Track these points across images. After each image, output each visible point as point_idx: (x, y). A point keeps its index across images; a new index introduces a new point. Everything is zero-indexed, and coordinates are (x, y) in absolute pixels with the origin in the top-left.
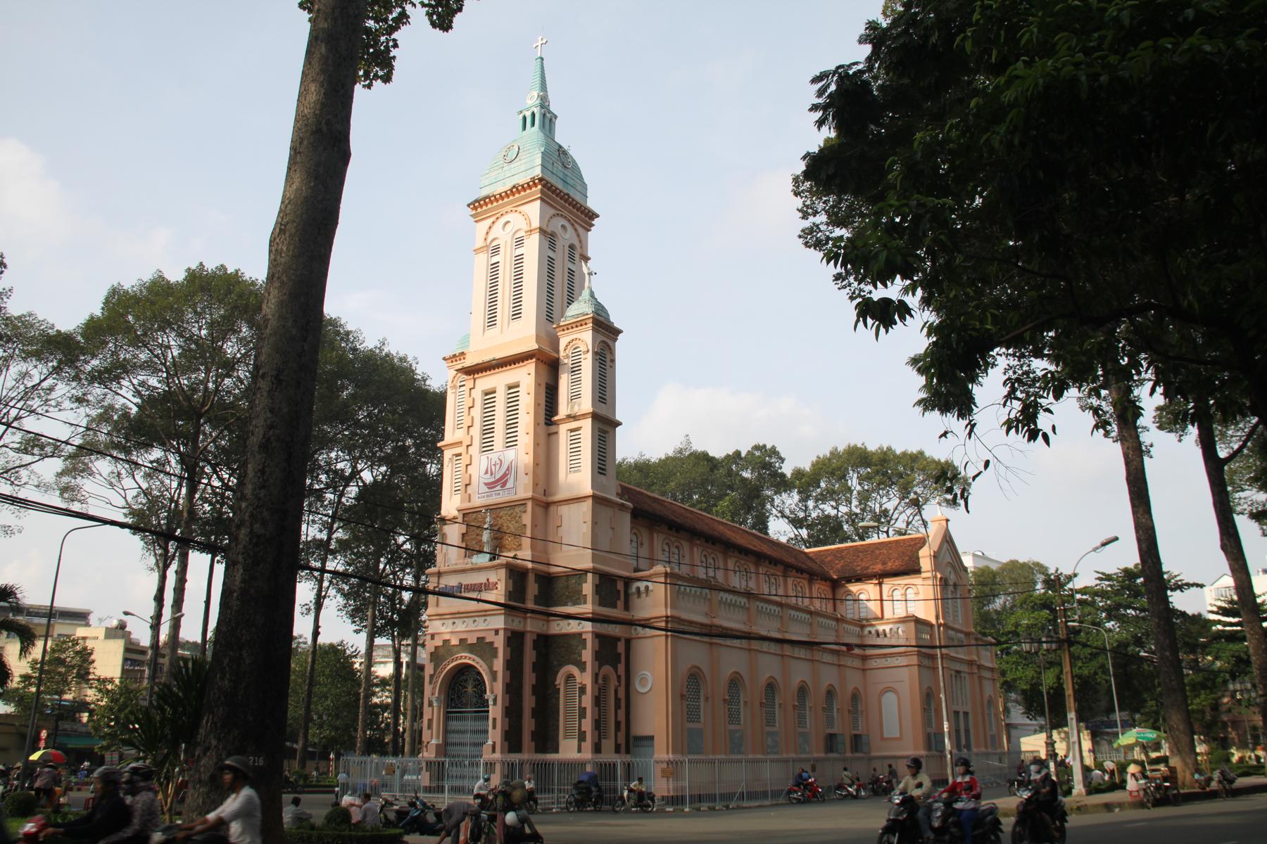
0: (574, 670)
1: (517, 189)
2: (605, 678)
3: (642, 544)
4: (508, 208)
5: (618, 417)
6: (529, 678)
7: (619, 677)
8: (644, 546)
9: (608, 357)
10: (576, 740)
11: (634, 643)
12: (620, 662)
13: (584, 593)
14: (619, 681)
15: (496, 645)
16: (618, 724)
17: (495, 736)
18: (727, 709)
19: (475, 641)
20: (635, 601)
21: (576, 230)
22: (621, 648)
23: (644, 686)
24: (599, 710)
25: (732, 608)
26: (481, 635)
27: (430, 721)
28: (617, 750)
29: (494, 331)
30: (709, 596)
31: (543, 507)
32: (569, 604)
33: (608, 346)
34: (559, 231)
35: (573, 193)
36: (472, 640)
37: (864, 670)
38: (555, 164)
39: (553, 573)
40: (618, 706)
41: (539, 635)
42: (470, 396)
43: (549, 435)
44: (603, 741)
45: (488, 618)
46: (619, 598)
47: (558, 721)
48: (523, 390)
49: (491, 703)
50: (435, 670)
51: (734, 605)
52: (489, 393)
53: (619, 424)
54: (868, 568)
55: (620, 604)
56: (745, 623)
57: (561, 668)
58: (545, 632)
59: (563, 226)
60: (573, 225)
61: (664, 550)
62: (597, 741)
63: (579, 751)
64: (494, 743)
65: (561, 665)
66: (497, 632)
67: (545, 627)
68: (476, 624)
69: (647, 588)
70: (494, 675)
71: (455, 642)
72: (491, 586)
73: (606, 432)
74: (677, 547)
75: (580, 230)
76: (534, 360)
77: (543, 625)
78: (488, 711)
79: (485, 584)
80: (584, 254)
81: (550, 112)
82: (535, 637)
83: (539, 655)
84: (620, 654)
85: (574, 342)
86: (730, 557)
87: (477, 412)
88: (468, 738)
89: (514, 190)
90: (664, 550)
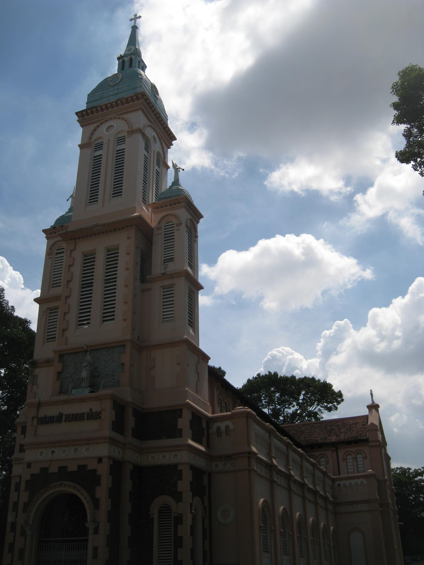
1: (122, 102)
13: (179, 427)
19: (75, 469)
43: (143, 291)
49: (91, 531)
54: (326, 438)
59: (154, 137)
66: (100, 460)
69: (227, 427)
71: (54, 469)
78: (87, 540)
87: (77, 270)
89: (119, 102)
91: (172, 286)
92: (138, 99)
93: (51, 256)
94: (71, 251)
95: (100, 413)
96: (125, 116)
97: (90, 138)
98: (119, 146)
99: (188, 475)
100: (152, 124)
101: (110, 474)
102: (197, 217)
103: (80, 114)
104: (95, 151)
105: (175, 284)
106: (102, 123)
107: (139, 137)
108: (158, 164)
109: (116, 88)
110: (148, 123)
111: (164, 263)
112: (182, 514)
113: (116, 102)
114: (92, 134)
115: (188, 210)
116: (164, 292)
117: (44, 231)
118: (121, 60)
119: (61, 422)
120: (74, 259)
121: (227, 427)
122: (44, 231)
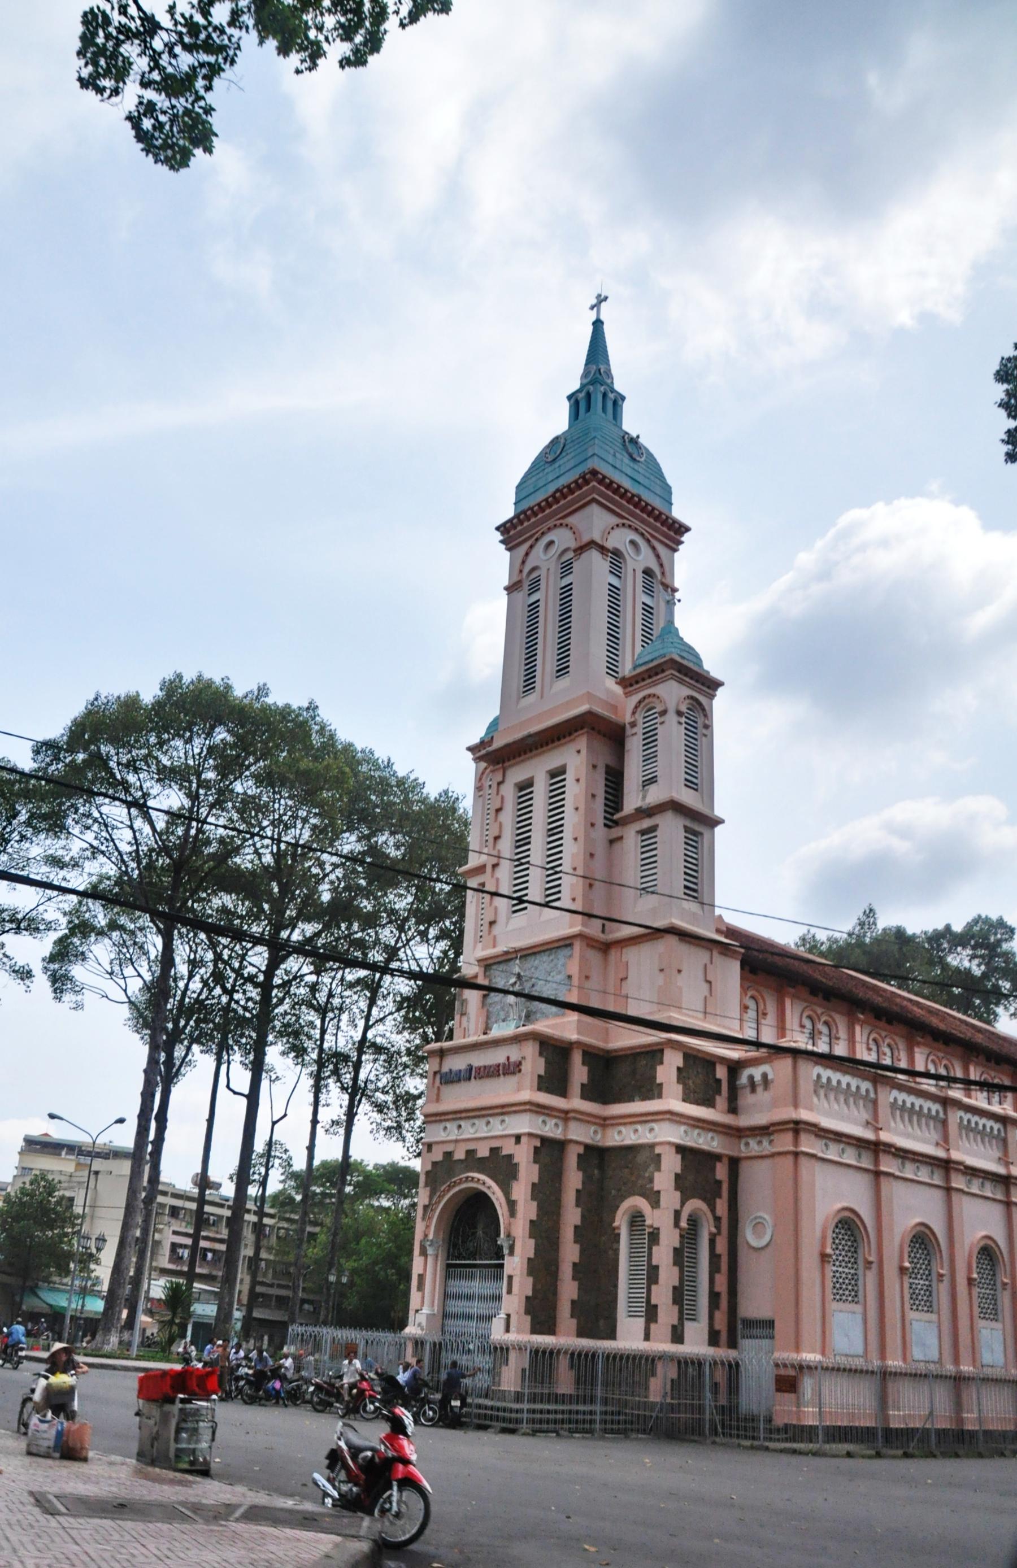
0: (640, 1202)
2: (694, 1221)
3: (765, 1014)
4: (551, 523)
5: (719, 812)
6: (572, 1216)
7: (717, 1219)
8: (769, 1017)
9: (701, 720)
10: (643, 1320)
11: (744, 1167)
12: (720, 1197)
13: (658, 1081)
14: (718, 1227)
15: (516, 1160)
16: (714, 1297)
17: (513, 1304)
18: (906, 1285)
20: (747, 1099)
21: (654, 548)
22: (721, 1172)
23: (759, 1236)
24: (681, 1272)
25: (932, 1123)
26: (495, 1144)
27: (421, 1277)
28: (714, 1339)
29: (532, 698)
30: (872, 1095)
31: (600, 949)
32: (637, 1098)
33: (700, 704)
34: (628, 551)
35: (647, 496)
36: (483, 1152)
37: (796, 1154)
38: (617, 455)
39: (616, 1051)
40: (714, 1267)
41: (587, 1147)
42: (498, 794)
43: (612, 842)
44: (688, 1325)
45: (506, 1118)
46: (719, 1092)
47: (616, 1286)
48: (570, 776)
49: (506, 1251)
50: (431, 1198)
51: (920, 1113)
52: (525, 786)
53: (719, 822)
55: (721, 1101)
56: (937, 1144)
57: (622, 1201)
58: (600, 1144)
59: (633, 542)
60: (648, 541)
61: (803, 1026)
62: (676, 1322)
63: (647, 1337)
64: (508, 1316)
65: (623, 1198)
66: (518, 1138)
67: (599, 1136)
68: (504, 1126)
69: (765, 1076)
70: (512, 1205)
71: (460, 1155)
72: (512, 1068)
73: (696, 833)
74: (826, 1023)
75: (661, 550)
76: (585, 730)
77: (595, 1132)
79: (504, 1064)
80: (667, 581)
81: (613, 391)
82: (581, 1150)
83: (587, 1180)
84: (719, 1183)
85: (647, 701)
86: (918, 1044)
88: (475, 1308)
89: (558, 495)
90: (803, 1026)
91: (653, 829)
92: (587, 482)
93: (481, 793)
94: (499, 784)
95: (520, 1063)
96: (570, 520)
97: (521, 571)
98: (564, 579)
99: (671, 1164)
100: (625, 521)
101: (535, 1162)
102: (709, 687)
103: (504, 528)
104: (529, 595)
105: (657, 826)
106: (537, 540)
107: (595, 555)
108: (648, 590)
109: (557, 465)
110: (615, 520)
111: (644, 786)
112: (658, 1229)
113: (553, 495)
114: (523, 562)
115: (681, 682)
116: (643, 841)
117: (469, 749)
118: (573, 400)
119: (470, 1079)
120: (502, 798)
121: (765, 1076)
122: (469, 749)
